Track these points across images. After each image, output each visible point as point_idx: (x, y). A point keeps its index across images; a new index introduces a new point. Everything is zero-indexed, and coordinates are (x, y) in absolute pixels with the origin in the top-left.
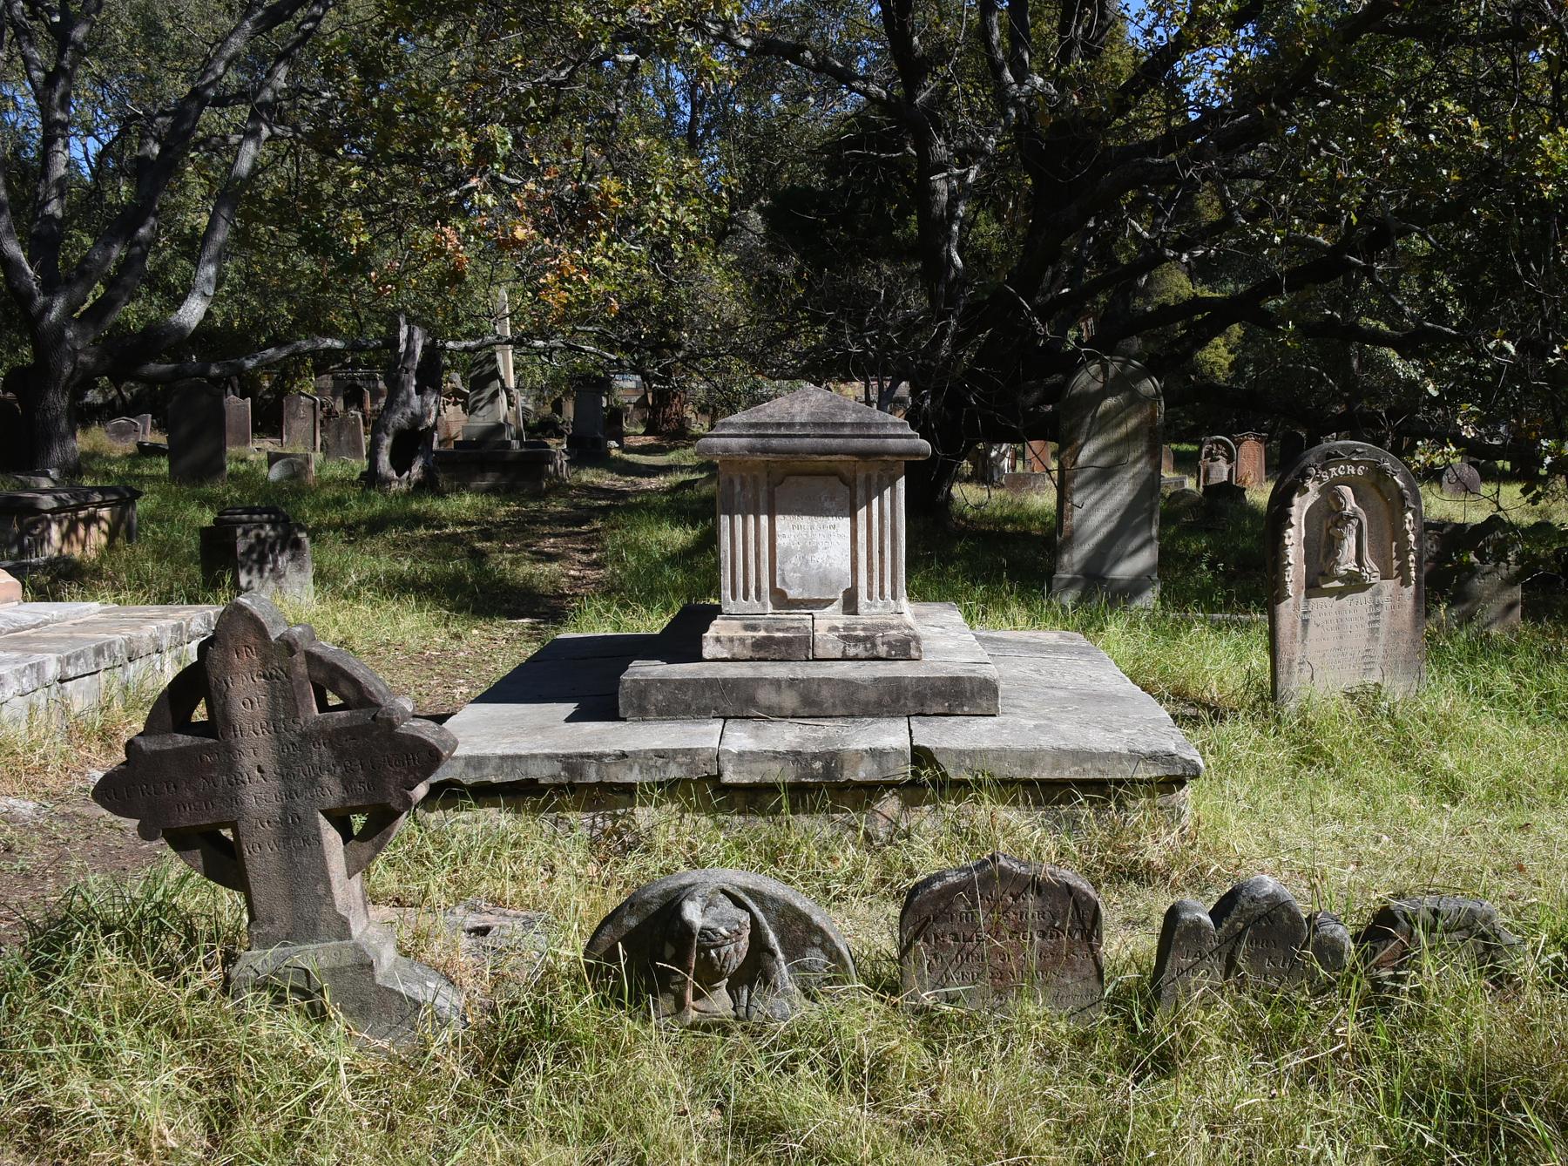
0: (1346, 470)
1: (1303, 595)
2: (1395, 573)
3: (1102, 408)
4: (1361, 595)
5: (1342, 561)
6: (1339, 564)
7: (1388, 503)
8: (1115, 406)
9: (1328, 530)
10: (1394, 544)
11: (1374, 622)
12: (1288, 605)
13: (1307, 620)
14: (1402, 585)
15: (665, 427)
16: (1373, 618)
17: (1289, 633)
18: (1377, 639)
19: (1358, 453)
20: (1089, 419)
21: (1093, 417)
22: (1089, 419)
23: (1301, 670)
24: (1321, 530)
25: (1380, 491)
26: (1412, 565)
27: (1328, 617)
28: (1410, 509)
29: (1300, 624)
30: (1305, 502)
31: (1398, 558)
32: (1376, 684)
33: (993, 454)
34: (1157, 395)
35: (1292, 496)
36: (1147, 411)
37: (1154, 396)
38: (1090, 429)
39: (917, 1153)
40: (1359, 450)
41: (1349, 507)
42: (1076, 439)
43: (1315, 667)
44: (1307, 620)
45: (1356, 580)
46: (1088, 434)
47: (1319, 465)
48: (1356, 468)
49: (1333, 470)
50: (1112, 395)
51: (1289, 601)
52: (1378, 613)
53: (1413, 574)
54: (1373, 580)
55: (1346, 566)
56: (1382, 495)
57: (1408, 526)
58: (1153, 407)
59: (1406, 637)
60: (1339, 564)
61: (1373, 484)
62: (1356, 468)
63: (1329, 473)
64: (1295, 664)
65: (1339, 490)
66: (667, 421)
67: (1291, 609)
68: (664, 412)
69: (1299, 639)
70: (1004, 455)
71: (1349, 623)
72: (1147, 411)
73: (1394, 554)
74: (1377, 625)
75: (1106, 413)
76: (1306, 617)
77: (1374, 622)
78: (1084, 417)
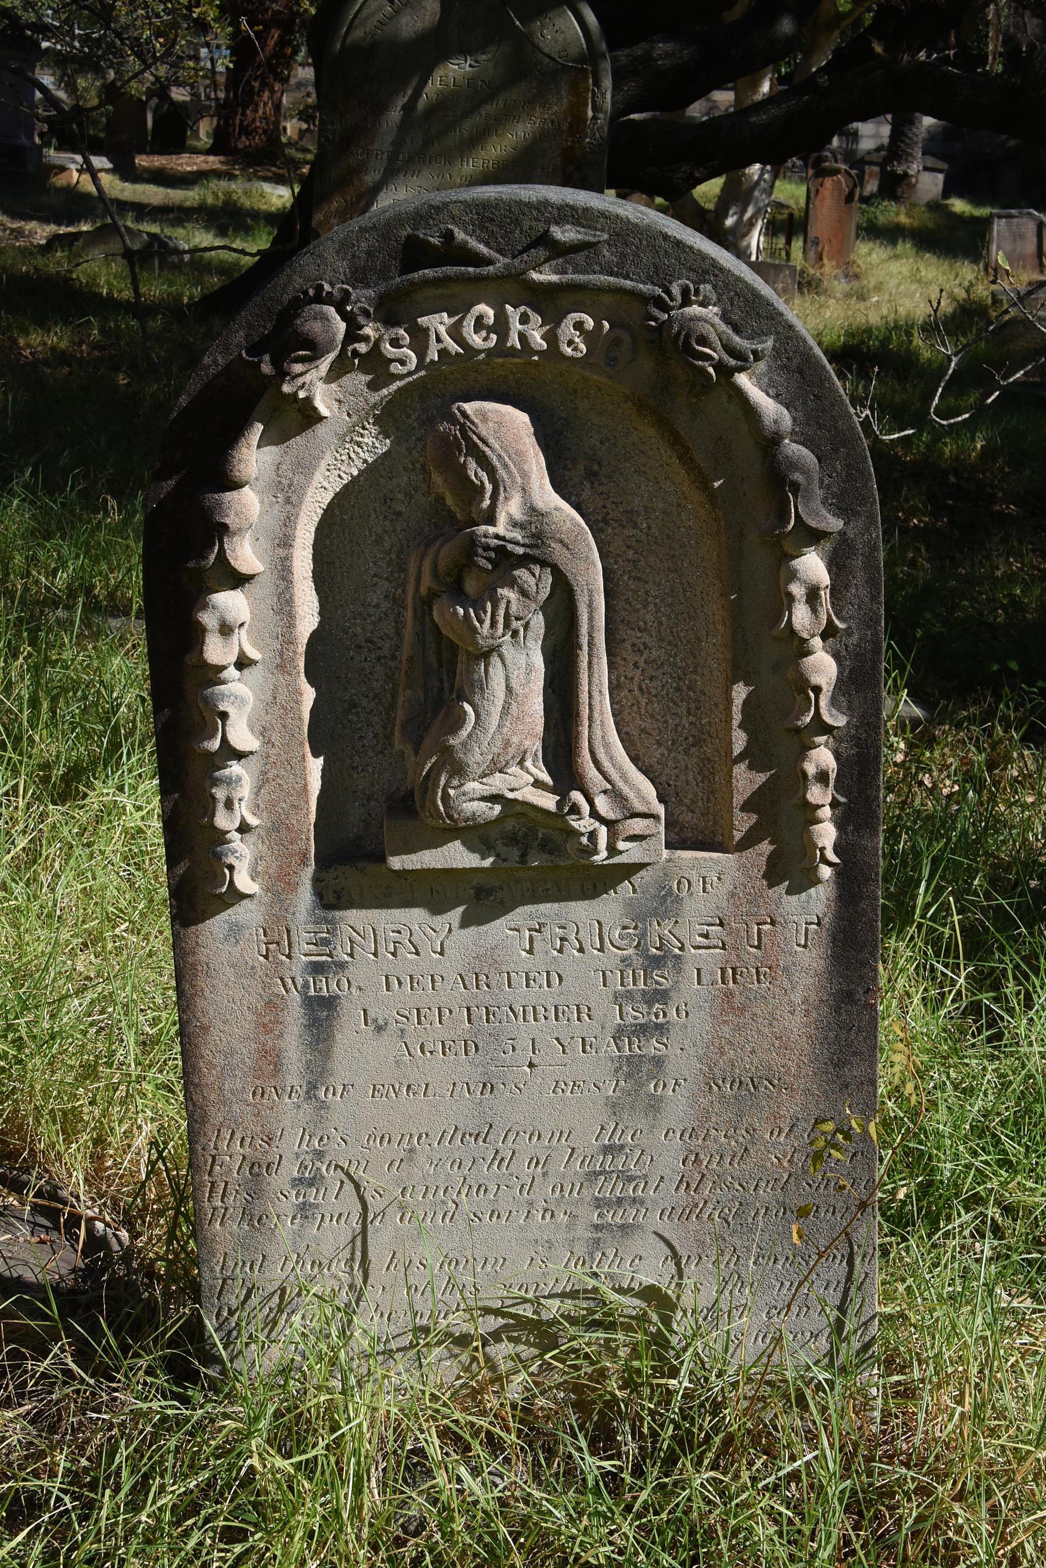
0: (501, 326)
1: (305, 896)
2: (743, 823)
3: (434, 86)
4: (580, 911)
5: (476, 758)
6: (459, 770)
7: (712, 496)
8: (471, 81)
9: (426, 604)
10: (740, 693)
11: (642, 1030)
12: (235, 930)
13: (329, 1003)
14: (773, 875)
15: (244, 142)
16: (634, 1015)
17: (246, 1053)
18: (655, 1106)
19: (558, 251)
20: (395, 115)
21: (409, 108)
22: (395, 115)
23: (305, 1210)
24: (398, 602)
25: (675, 439)
26: (816, 794)
27: (425, 997)
28: (814, 537)
29: (295, 1015)
30: (306, 467)
31: (754, 757)
32: (650, 1293)
33: (729, 222)
34: (591, 57)
35: (234, 434)
36: (558, 106)
37: (582, 59)
38: (398, 143)
39: (1038, 1003)
40: (565, 234)
41: (511, 508)
42: (361, 169)
43: (375, 1204)
44: (329, 1003)
45: (547, 847)
46: (393, 157)
47: (362, 297)
48: (553, 319)
49: (439, 323)
50: (464, 51)
51: (239, 913)
52: (660, 996)
53: (826, 834)
54: (630, 852)
55: (497, 783)
56: (685, 457)
57: (801, 616)
58: (578, 93)
59: (791, 1107)
60: (459, 770)
61: (641, 406)
62: (553, 319)
63: (420, 339)
64: (280, 1180)
65: (465, 425)
66: (247, 131)
67: (252, 950)
68: (244, 114)
69: (294, 1076)
70: (751, 224)
71: (525, 1031)
72: (558, 106)
73: (739, 741)
74: (653, 1047)
75: (443, 104)
76: (325, 987)
77: (642, 1030)
78: (381, 108)
